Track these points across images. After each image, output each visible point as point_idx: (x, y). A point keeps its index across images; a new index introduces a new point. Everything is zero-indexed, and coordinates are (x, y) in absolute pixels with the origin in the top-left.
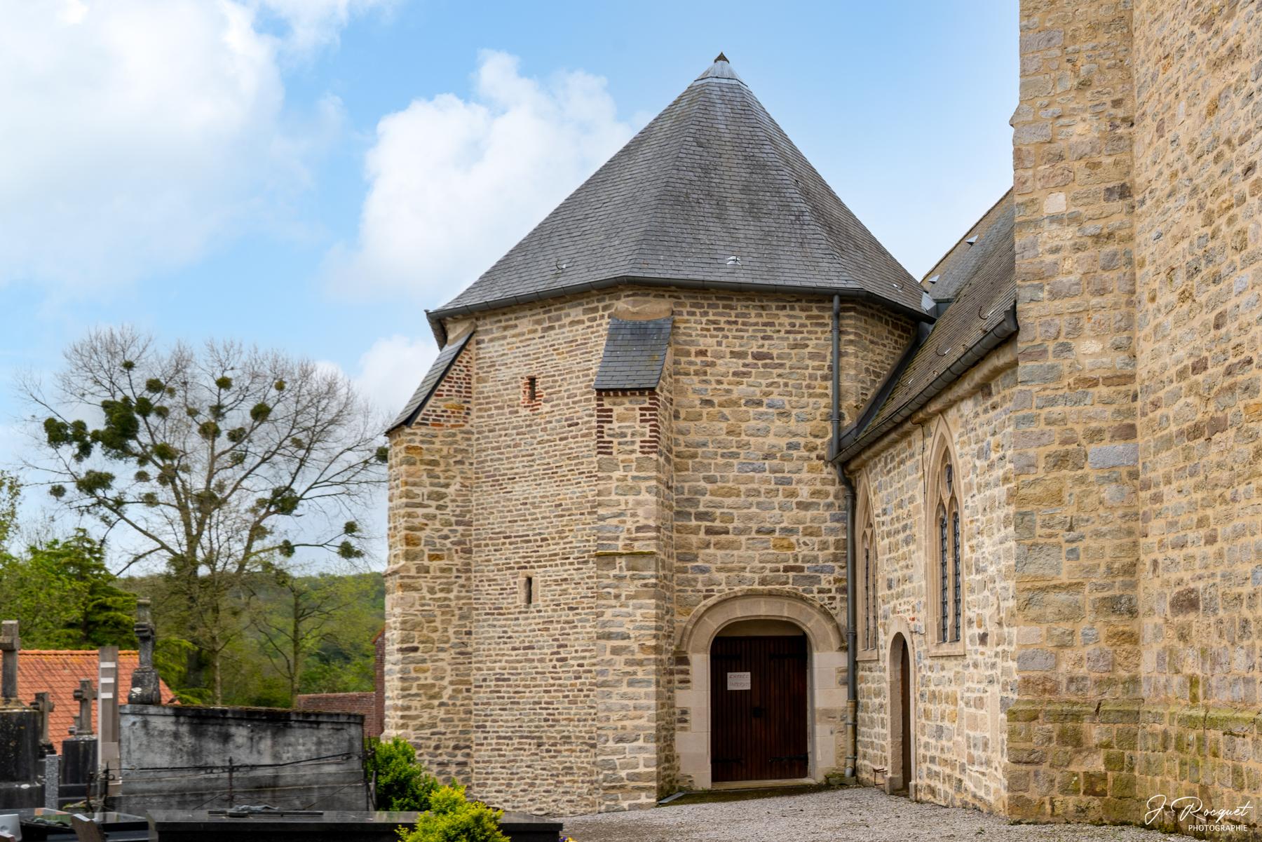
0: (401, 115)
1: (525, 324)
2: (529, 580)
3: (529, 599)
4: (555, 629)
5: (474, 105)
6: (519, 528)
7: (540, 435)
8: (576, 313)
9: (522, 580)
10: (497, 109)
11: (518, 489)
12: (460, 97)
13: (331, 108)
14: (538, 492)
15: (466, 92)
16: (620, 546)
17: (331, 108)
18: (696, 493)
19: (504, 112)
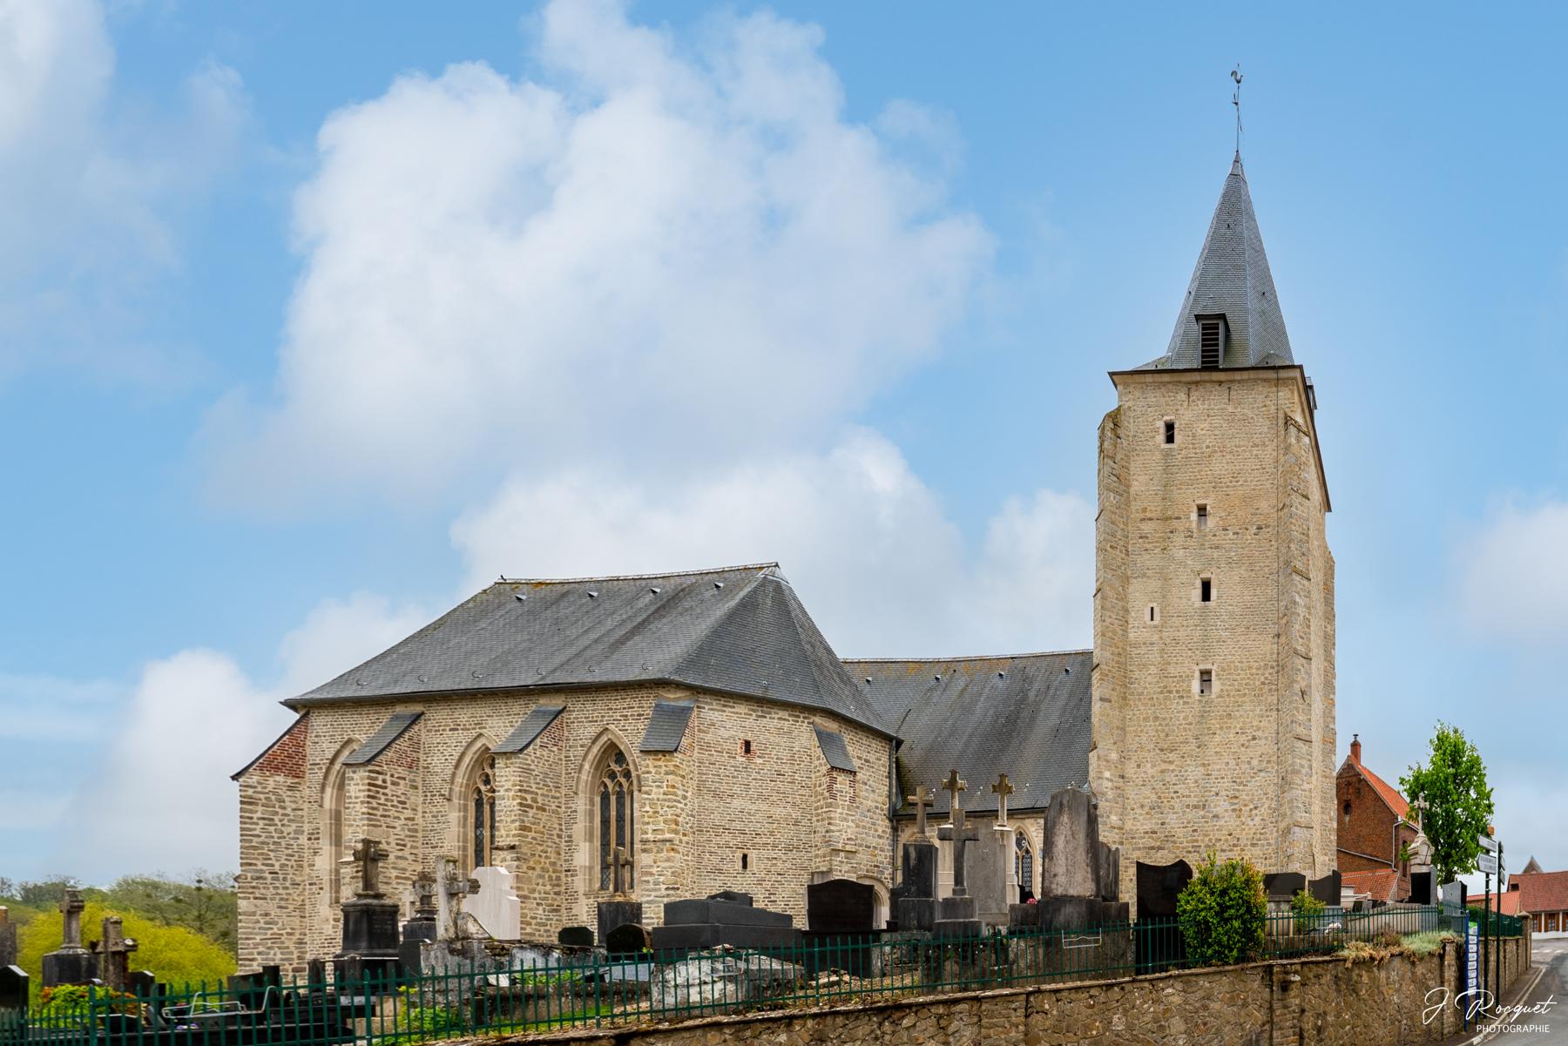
0: (371, 109)
1: (742, 709)
2: (745, 857)
3: (745, 866)
4: (767, 885)
5: (531, 86)
6: (738, 825)
7: (754, 775)
8: (785, 714)
9: (739, 855)
10: (581, 97)
11: (736, 803)
12: (499, 67)
13: (216, 91)
14: (754, 807)
15: (515, 59)
16: (840, 846)
17: (216, 91)
18: (337, 902)
19: (596, 103)
